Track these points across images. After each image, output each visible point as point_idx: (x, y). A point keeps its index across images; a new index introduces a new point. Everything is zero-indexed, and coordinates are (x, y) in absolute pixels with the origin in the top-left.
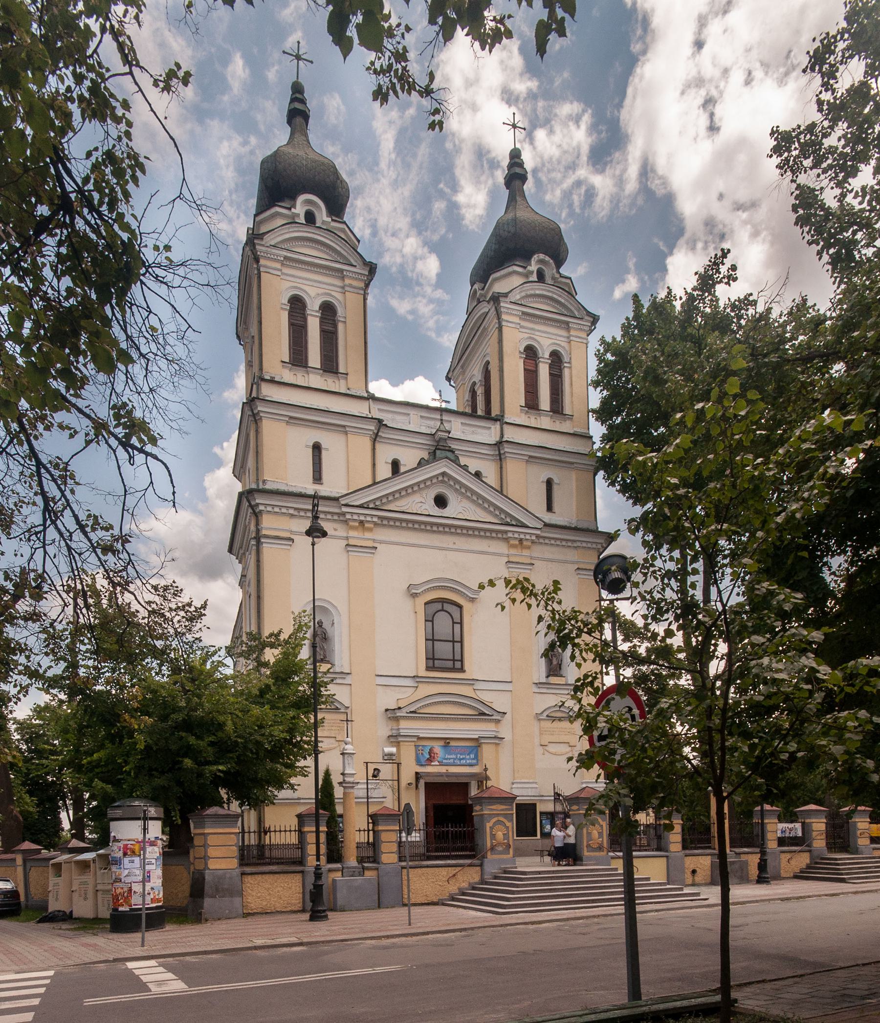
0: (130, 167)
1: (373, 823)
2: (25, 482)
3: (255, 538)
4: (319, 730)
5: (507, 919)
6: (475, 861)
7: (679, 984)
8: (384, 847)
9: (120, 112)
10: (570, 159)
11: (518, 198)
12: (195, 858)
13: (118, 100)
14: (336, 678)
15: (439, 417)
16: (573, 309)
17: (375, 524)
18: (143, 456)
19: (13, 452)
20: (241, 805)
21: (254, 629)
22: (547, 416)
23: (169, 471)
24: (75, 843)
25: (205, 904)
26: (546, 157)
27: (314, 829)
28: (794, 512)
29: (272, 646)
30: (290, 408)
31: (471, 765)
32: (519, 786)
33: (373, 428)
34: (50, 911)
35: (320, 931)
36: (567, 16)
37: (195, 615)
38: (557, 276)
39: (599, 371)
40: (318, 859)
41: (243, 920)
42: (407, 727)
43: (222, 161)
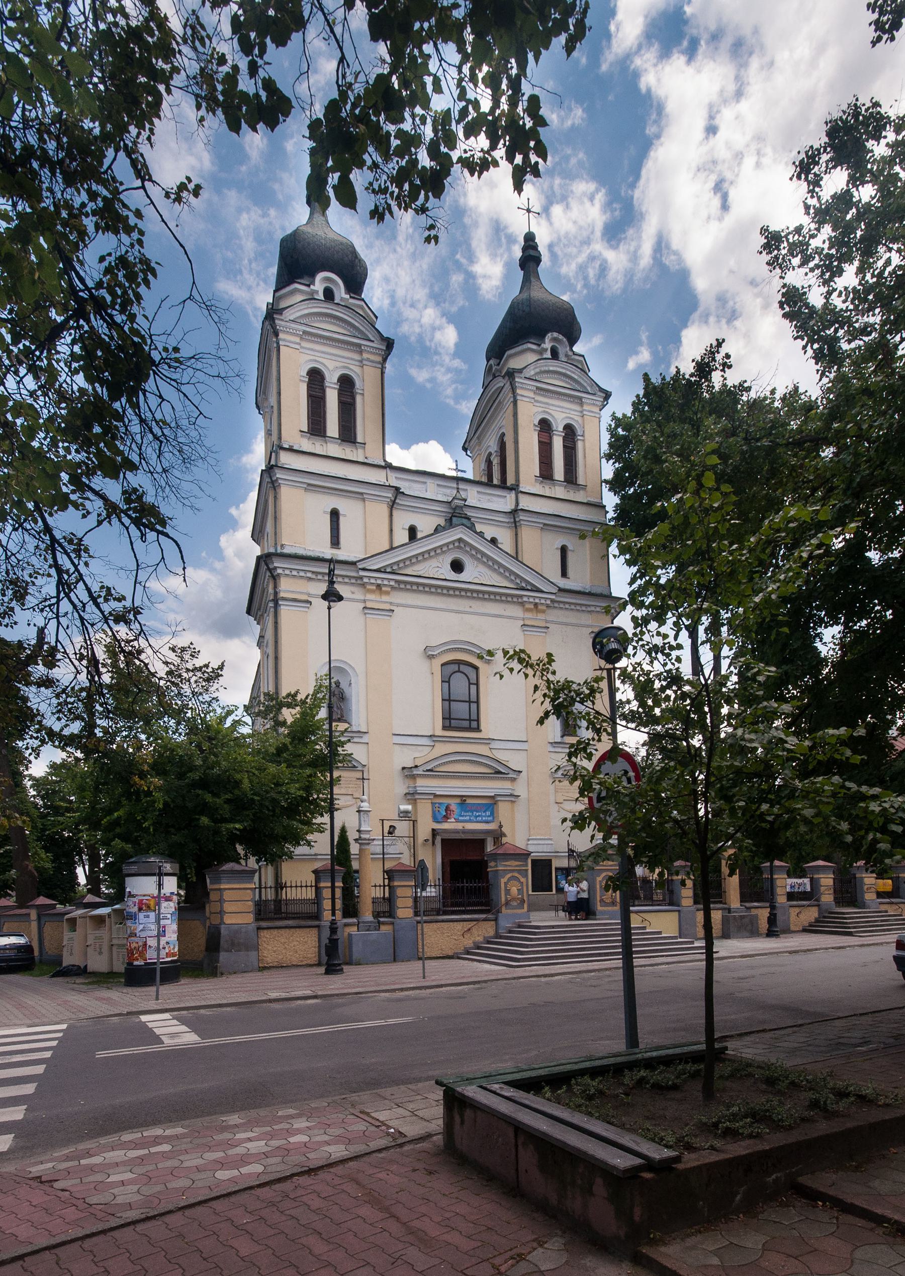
0: (141, 271)
1: (389, 879)
2: (40, 555)
3: (273, 600)
4: (335, 788)
5: (520, 972)
6: (490, 916)
7: (683, 1033)
8: (400, 903)
9: (133, 220)
10: (585, 234)
11: (533, 279)
12: (211, 913)
13: (130, 210)
14: (352, 737)
15: (455, 486)
16: (585, 384)
17: (392, 587)
18: (154, 534)
19: (29, 527)
20: (258, 861)
21: (272, 689)
22: (560, 485)
23: (180, 549)
24: (90, 898)
25: (221, 958)
26: (562, 233)
27: (329, 884)
28: (771, 593)
29: (289, 706)
30: (298, 474)
31: (487, 822)
32: (535, 842)
33: (390, 495)
34: (64, 964)
35: (335, 984)
36: (540, 161)
37: (213, 675)
38: (570, 353)
39: (611, 445)
40: (333, 914)
41: (260, 974)
42: (424, 785)
43: (241, 232)
